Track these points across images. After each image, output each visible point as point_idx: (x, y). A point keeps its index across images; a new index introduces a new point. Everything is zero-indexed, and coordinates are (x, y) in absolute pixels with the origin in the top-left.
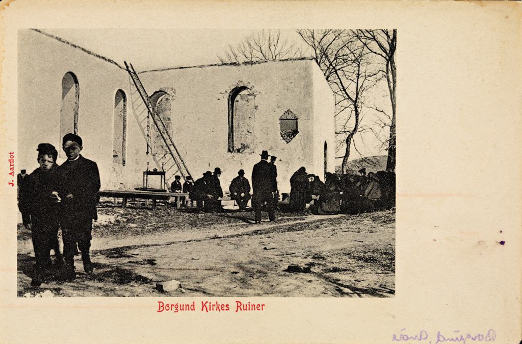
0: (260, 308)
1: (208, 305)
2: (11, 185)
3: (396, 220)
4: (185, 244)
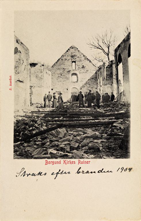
0: (88, 163)
1: (66, 162)
2: (10, 90)
3: (29, 48)
4: (91, 48)
